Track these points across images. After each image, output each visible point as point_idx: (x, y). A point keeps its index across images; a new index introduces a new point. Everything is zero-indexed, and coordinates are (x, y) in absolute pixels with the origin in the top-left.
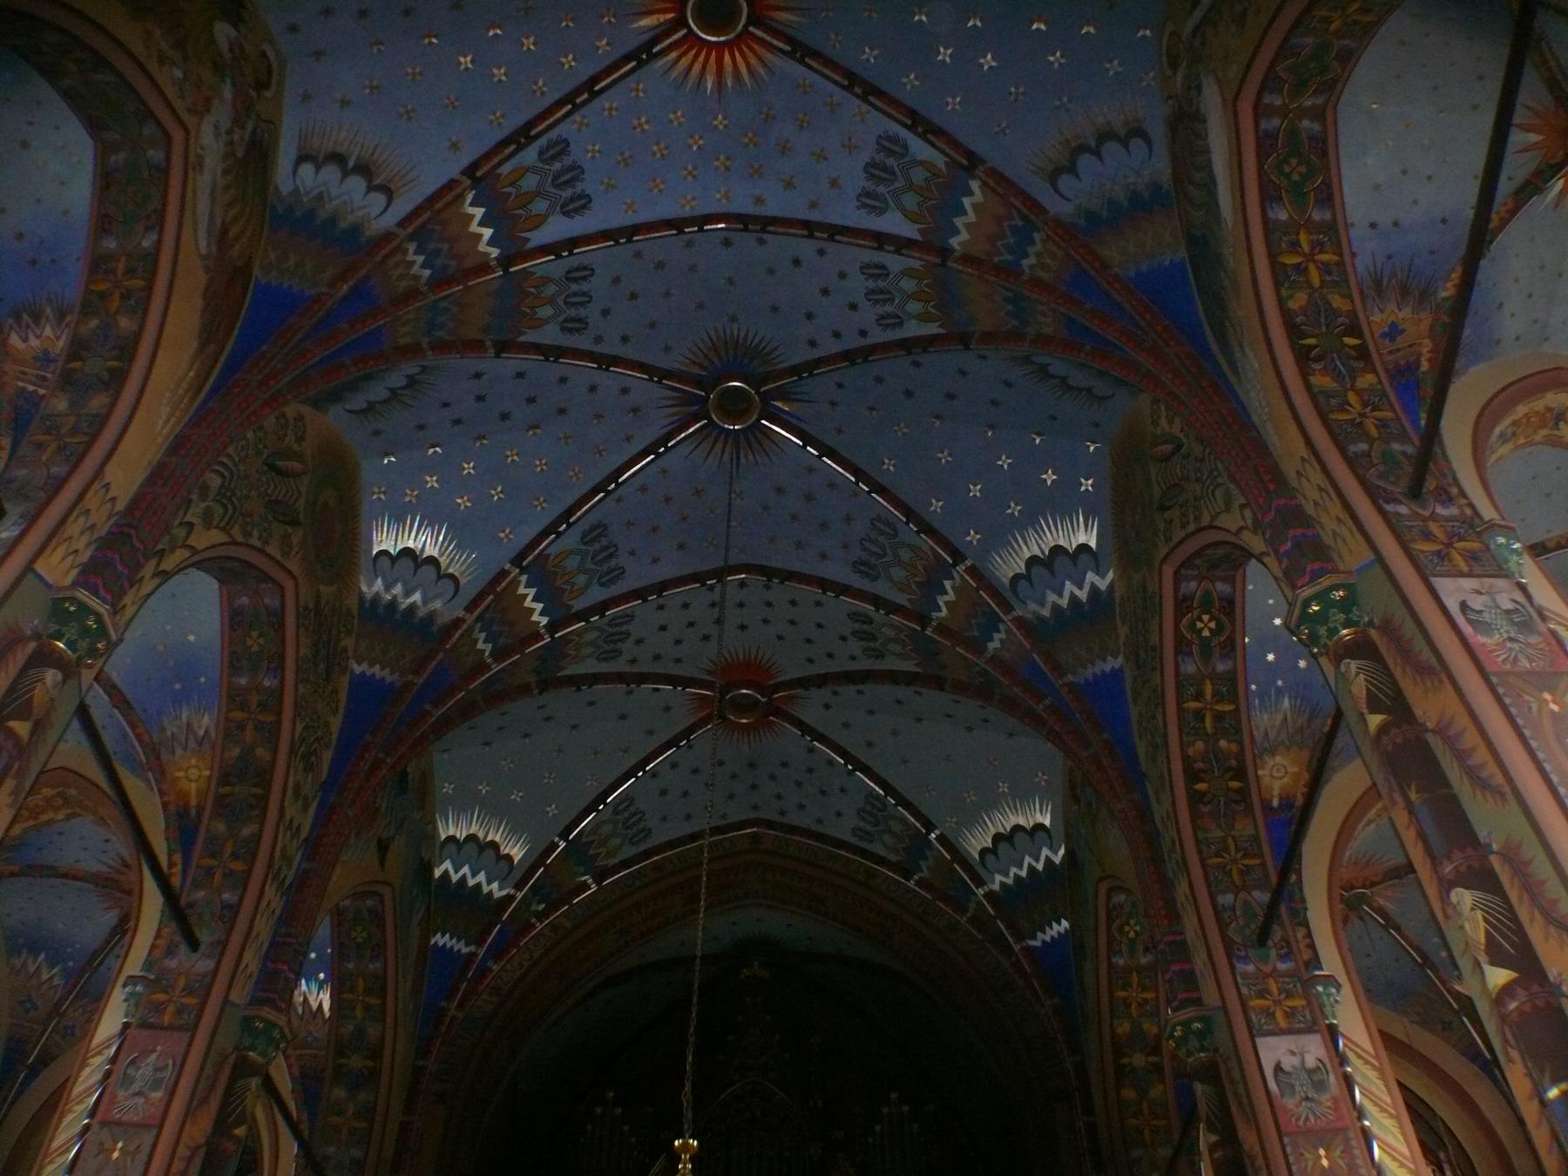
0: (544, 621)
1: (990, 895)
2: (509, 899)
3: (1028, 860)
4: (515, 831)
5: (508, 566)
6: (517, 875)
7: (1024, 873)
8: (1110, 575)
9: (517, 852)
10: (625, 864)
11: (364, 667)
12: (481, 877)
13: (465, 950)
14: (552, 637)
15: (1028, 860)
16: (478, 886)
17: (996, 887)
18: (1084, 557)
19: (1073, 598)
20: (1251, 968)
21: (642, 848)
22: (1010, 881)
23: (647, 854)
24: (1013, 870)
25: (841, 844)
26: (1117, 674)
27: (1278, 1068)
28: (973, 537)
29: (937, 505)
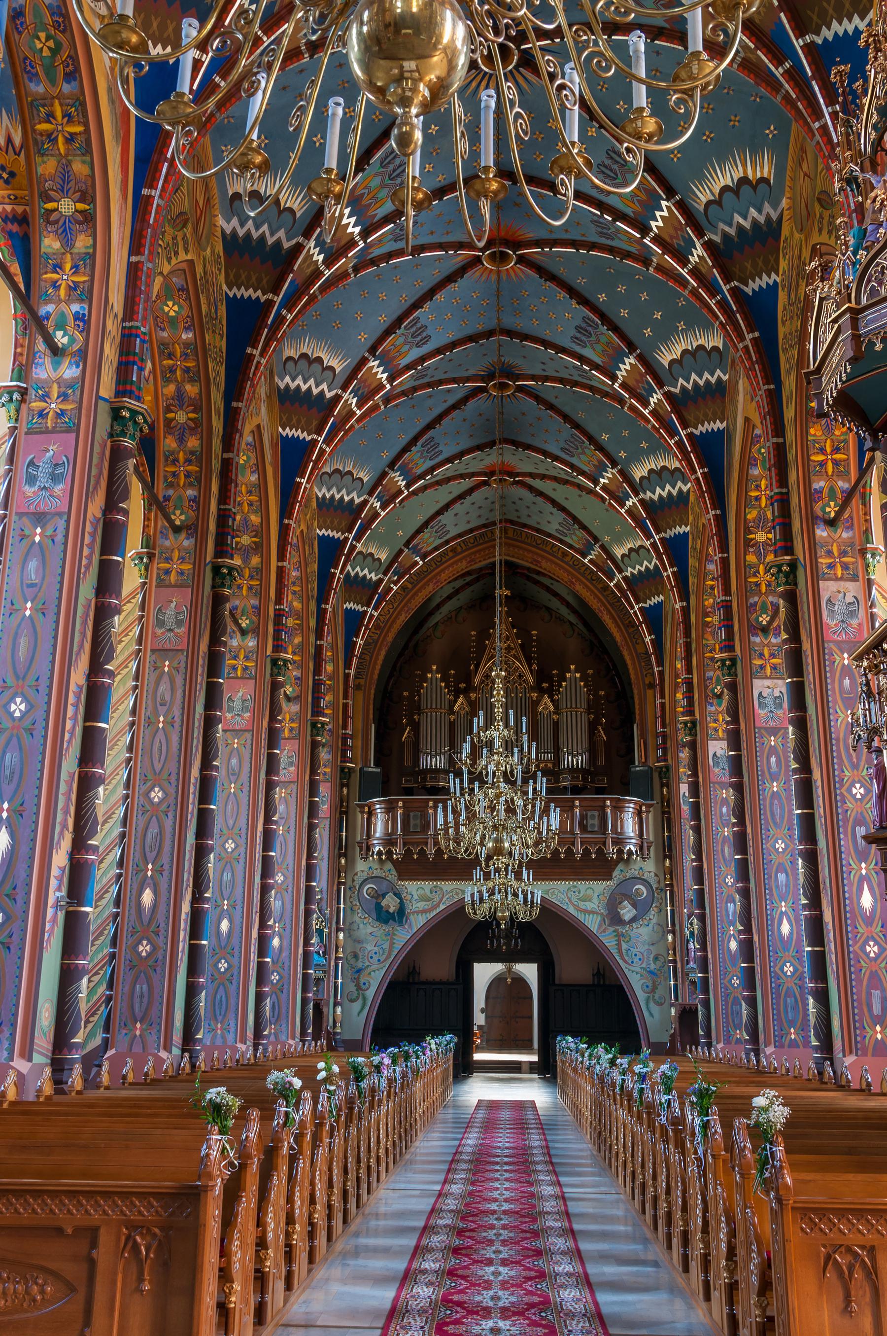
0: (357, 230)
1: (625, 578)
2: (380, 581)
3: (645, 563)
4: (381, 546)
5: (367, 355)
6: (383, 568)
7: (643, 569)
8: (689, 485)
9: (383, 556)
10: (436, 549)
11: (324, 531)
12: (366, 571)
13: (308, 438)
14: (365, 242)
15: (645, 563)
16: (365, 576)
17: (629, 574)
18: (677, 473)
19: (669, 493)
20: (713, 709)
21: (445, 538)
22: (635, 572)
23: (447, 542)
24: (638, 567)
25: (550, 535)
26: (686, 535)
27: (715, 755)
28: (622, 454)
29: (624, 313)
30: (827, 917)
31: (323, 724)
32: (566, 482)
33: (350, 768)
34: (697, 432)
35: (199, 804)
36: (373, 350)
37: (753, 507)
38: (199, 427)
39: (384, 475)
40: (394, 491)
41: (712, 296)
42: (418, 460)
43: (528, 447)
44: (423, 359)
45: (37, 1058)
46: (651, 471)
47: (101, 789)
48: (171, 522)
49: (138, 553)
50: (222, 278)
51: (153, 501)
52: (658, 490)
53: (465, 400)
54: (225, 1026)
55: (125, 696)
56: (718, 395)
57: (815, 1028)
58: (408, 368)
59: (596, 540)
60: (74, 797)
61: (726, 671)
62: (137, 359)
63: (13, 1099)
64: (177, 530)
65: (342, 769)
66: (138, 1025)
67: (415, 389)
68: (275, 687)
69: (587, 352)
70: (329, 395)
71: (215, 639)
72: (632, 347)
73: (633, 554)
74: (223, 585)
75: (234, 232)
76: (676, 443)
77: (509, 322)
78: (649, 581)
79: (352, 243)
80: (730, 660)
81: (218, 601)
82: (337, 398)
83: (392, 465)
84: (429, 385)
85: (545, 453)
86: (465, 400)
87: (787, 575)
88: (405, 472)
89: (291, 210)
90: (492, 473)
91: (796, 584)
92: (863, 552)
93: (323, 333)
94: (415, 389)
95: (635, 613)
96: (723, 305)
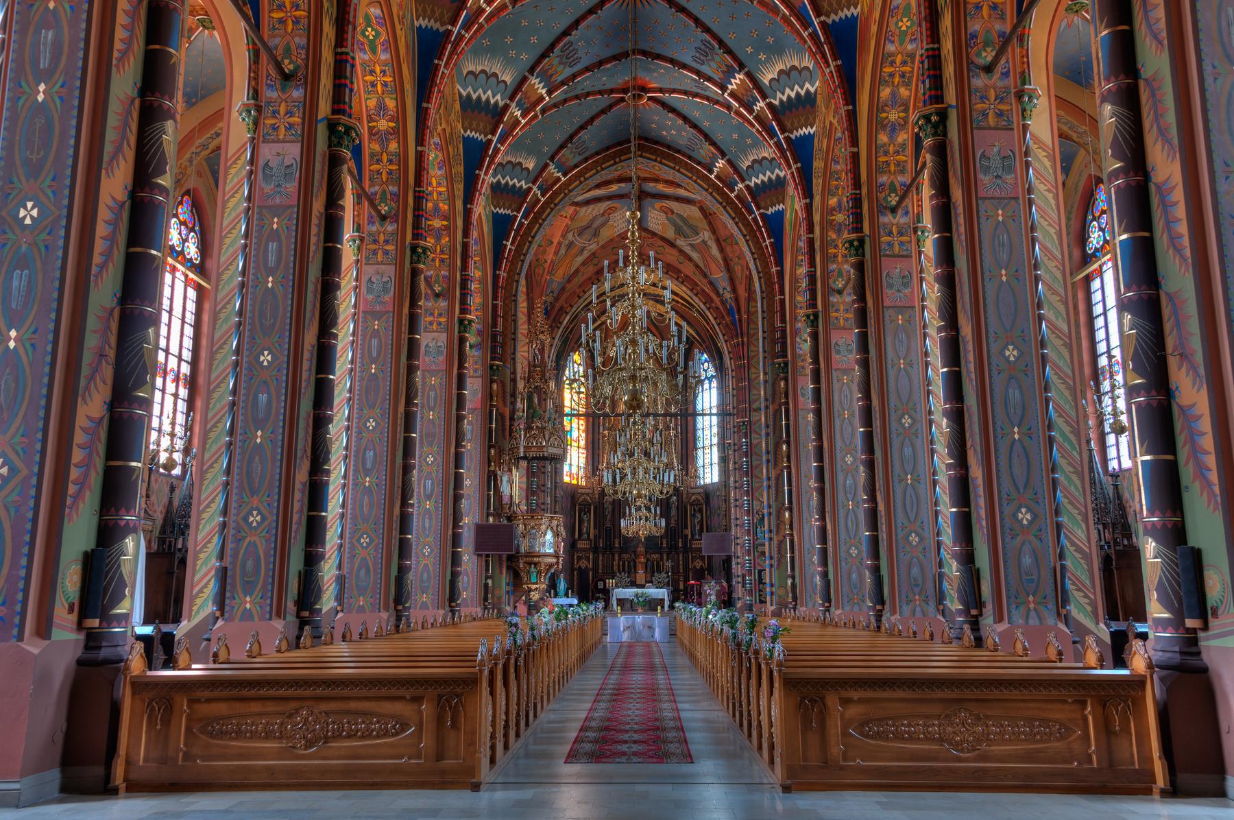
13: (442, 29)
21: (585, 155)
30: (829, 527)
31: (470, 321)
33: (498, 366)
34: (830, 21)
35: (317, 373)
36: (552, 158)
37: (834, 195)
38: (399, 132)
39: (524, 80)
40: (533, 99)
41: (772, 138)
42: (567, 155)
43: (658, 57)
44: (574, 76)
45: (58, 634)
46: (781, 72)
48: (378, 212)
49: (244, 105)
50: (460, 126)
51: (360, 195)
53: (611, 107)
56: (806, 104)
57: (1160, 588)
58: (563, 83)
59: (742, 66)
60: (310, 431)
61: (853, 252)
62: (348, 82)
63: (136, 673)
64: (437, 296)
65: (491, 366)
66: (1031, 598)
67: (565, 101)
68: (462, 341)
69: (705, 69)
71: (413, 303)
72: (742, 66)
73: (756, 165)
74: (419, 261)
75: (469, 95)
76: (810, 34)
77: (642, 46)
80: (937, 114)
81: (415, 273)
82: (530, 189)
83: (532, 70)
84: (577, 97)
86: (611, 107)
88: (546, 77)
89: (505, 82)
90: (625, 91)
91: (864, 256)
92: (1019, 95)
93: (493, 51)
94: (565, 101)
95: (755, 219)
96: (814, 36)
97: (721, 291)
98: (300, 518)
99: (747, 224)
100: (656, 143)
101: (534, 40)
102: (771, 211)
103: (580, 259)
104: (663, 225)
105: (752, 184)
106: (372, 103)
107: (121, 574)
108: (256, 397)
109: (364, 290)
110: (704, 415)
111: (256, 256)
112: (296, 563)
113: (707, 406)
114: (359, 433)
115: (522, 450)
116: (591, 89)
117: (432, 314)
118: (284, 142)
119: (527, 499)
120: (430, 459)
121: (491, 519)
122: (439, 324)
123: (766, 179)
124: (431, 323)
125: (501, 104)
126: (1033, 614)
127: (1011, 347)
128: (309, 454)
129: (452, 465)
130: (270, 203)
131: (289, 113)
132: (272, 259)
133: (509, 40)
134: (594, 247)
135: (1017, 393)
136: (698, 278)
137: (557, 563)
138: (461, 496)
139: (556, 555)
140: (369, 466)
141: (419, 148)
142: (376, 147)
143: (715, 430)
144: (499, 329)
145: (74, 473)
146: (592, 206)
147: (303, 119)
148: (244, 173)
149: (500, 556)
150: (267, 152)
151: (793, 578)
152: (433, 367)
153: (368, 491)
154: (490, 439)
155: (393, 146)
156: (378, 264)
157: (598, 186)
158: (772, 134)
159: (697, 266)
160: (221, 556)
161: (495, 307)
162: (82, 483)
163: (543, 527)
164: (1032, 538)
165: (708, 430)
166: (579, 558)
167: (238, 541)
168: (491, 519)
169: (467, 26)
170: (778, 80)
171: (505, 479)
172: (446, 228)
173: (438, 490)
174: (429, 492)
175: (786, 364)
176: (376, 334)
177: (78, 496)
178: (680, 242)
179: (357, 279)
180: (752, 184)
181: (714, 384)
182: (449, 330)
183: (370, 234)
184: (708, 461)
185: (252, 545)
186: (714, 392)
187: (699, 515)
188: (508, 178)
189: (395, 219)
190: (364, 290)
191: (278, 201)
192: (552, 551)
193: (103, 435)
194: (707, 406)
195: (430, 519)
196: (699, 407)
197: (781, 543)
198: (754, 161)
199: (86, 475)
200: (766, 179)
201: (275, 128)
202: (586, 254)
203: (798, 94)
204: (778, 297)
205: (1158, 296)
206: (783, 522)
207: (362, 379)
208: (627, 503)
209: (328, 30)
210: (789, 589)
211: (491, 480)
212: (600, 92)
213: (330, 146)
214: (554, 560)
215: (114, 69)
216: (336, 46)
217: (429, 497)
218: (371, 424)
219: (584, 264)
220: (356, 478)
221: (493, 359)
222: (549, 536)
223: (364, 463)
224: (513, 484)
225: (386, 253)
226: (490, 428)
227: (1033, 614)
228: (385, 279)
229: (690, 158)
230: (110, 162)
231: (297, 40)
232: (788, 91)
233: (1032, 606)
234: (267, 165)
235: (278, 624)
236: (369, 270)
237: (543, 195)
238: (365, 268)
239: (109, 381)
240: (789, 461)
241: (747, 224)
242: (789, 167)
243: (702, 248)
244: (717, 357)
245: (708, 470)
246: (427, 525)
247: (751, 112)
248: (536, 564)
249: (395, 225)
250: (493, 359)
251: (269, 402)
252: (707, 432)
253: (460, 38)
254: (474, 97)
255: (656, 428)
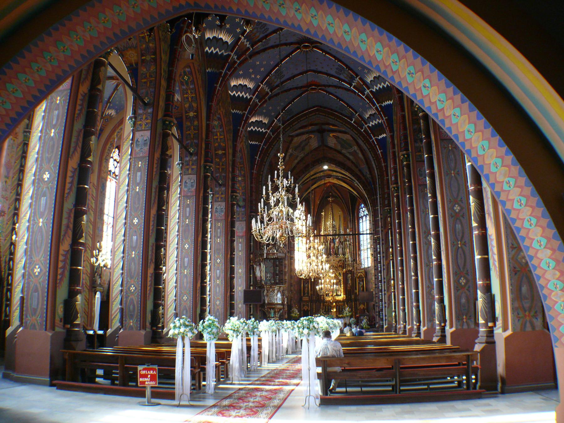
23: (293, 117)
32: (339, 87)
47: (85, 216)
52: (379, 85)
54: (463, 243)
55: (176, 201)
58: (278, 86)
69: (342, 77)
70: (249, 97)
73: (372, 117)
78: (378, 129)
79: (249, 49)
85: (328, 75)
87: (396, 190)
89: (250, 88)
95: (373, 141)
97: (365, 174)
98: (150, 289)
99: (369, 144)
100: (325, 108)
101: (262, 69)
102: (380, 137)
103: (296, 161)
104: (335, 144)
105: (371, 125)
106: (187, 105)
107: (76, 310)
108: (132, 238)
109: (183, 187)
110: (363, 234)
111: (133, 178)
112: (150, 306)
113: (365, 229)
114: (182, 250)
115: (265, 255)
116: (291, 87)
117: (218, 194)
118: (144, 130)
119: (274, 277)
120: (219, 261)
121: (252, 288)
122: (222, 198)
123: (377, 123)
124: (218, 198)
125: (249, 97)
126: (465, 324)
127: (457, 206)
128: (154, 261)
129: (229, 263)
130: (138, 156)
131: (146, 119)
132: (138, 179)
133: (251, 71)
134: (302, 155)
135: (460, 226)
136: (353, 168)
137: (283, 308)
138: (234, 278)
139: (283, 304)
140: (186, 265)
141: (208, 122)
142: (189, 124)
143: (369, 241)
144: (254, 198)
145: (60, 271)
146: (299, 137)
147: (152, 121)
148: (129, 144)
149: (256, 305)
150: (138, 134)
151: (395, 312)
152: (219, 218)
153: (186, 276)
154: (251, 250)
155: (196, 123)
156: (189, 174)
157: (300, 128)
158: (374, 104)
159: (352, 162)
160: (121, 304)
161: (251, 187)
162: (63, 274)
163: (276, 291)
164: (466, 291)
165: (366, 241)
166: (304, 305)
167: (127, 297)
168: (252, 288)
169: (229, 69)
170: (374, 81)
171: (258, 268)
172: (225, 154)
173: (223, 275)
174: (218, 275)
175: (390, 210)
176: (188, 206)
177: (61, 279)
178: (344, 151)
179: (180, 182)
180: (371, 125)
181: (368, 218)
182: (226, 200)
183: (186, 161)
184: (366, 256)
185: (132, 299)
186: (368, 222)
187: (361, 283)
188: (256, 128)
189: (196, 154)
190: (183, 187)
191: (141, 155)
192: (280, 302)
193: (69, 256)
194: (365, 229)
195: (219, 288)
196: (361, 230)
197: (390, 296)
198: (370, 115)
199: (63, 272)
200: (377, 123)
201: (141, 125)
202: (299, 159)
203: (383, 86)
204: (385, 178)
205: (482, 189)
206: (391, 286)
207: (183, 226)
208: (320, 278)
209: (164, 83)
210: (393, 317)
211: (250, 269)
212: (296, 88)
213: (163, 130)
214: (282, 307)
215: (75, 121)
216: (167, 89)
217: (218, 278)
218: (187, 246)
219: (298, 163)
220: (181, 271)
221: (251, 212)
222: (279, 295)
223: (184, 264)
224: (261, 272)
225: (192, 169)
226: (251, 245)
227: (465, 324)
228: (192, 181)
229: (341, 114)
230: (72, 155)
231: (151, 89)
232: (379, 85)
233: (465, 320)
234: (137, 140)
235: (143, 332)
236: (186, 177)
237: (273, 135)
238: (184, 177)
239: (71, 236)
240: (393, 256)
241: (369, 144)
242: (383, 119)
243: (354, 154)
244: (366, 206)
245: (366, 261)
246: (218, 291)
247: (364, 95)
248: (273, 308)
249: (196, 157)
250: (251, 212)
251: (137, 239)
252: (365, 242)
253: (226, 74)
254: (237, 95)
255: (340, 242)
